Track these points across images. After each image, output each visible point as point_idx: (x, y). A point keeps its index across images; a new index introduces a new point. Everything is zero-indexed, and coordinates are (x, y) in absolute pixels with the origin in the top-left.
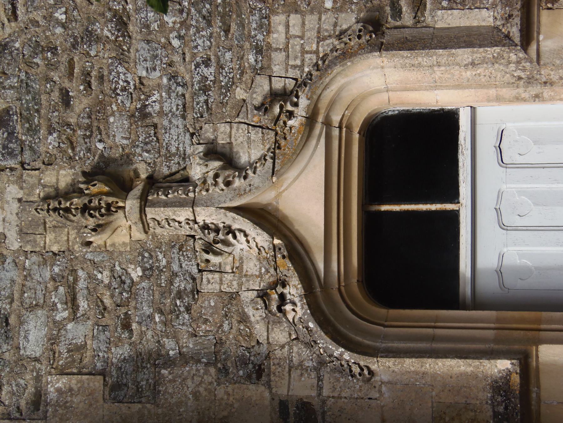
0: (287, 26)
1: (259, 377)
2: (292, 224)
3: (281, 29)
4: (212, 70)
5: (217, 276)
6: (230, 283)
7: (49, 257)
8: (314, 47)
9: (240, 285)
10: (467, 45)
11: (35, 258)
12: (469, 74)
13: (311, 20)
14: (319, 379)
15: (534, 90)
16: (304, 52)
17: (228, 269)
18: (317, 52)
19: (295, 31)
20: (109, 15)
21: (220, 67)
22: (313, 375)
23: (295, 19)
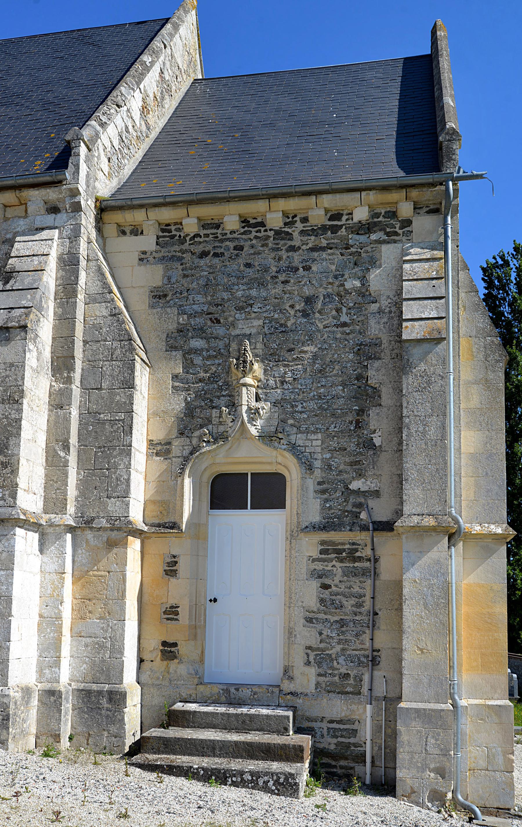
0: (317, 440)
1: (180, 434)
2: (171, 208)
3: (316, 437)
4: (300, 410)
5: (218, 415)
6: (215, 421)
7: (227, 346)
8: (307, 451)
9: (214, 425)
10: (248, 756)
11: (227, 342)
12: (295, 512)
13: (319, 449)
14: (179, 457)
15: (289, 537)
16: (305, 446)
17: (221, 420)
18: (305, 452)
19: (315, 443)
20: (324, 366)
21: (301, 412)
22: (180, 455)
23: (319, 443)
